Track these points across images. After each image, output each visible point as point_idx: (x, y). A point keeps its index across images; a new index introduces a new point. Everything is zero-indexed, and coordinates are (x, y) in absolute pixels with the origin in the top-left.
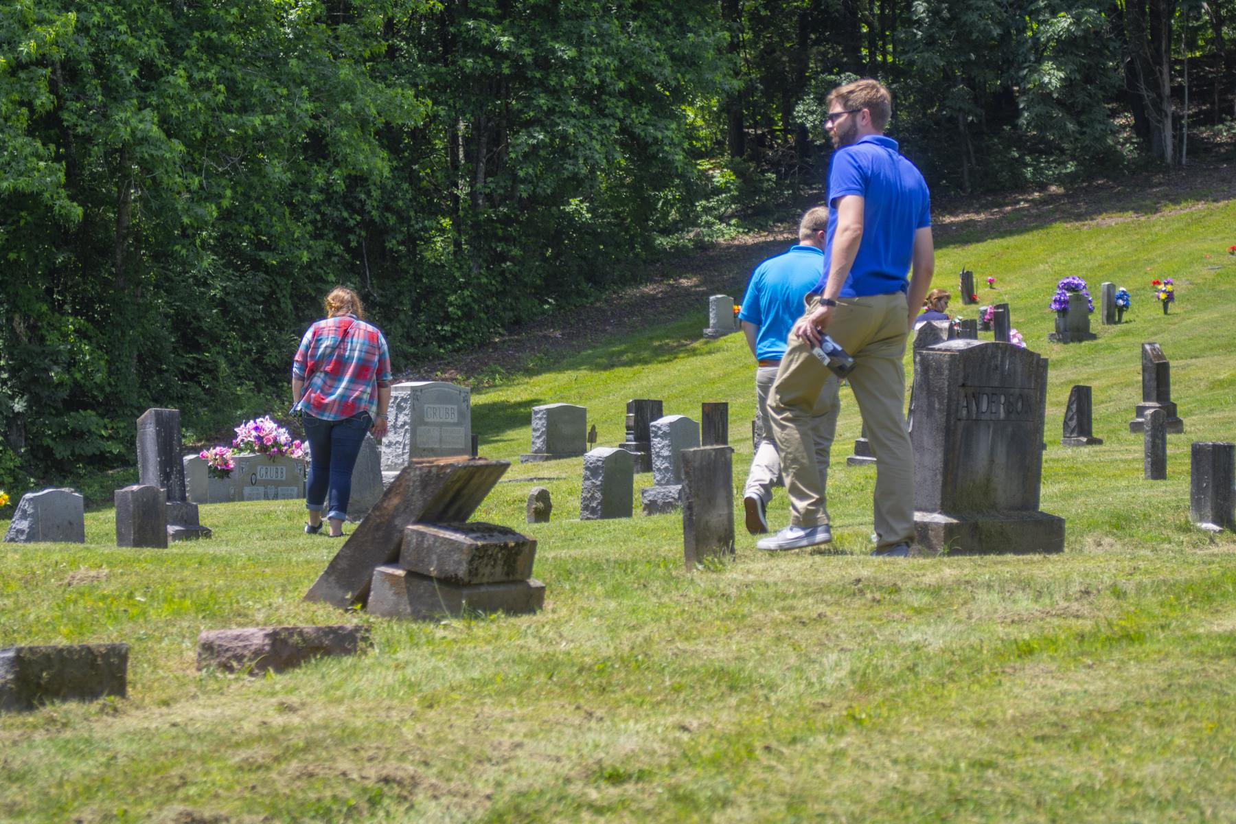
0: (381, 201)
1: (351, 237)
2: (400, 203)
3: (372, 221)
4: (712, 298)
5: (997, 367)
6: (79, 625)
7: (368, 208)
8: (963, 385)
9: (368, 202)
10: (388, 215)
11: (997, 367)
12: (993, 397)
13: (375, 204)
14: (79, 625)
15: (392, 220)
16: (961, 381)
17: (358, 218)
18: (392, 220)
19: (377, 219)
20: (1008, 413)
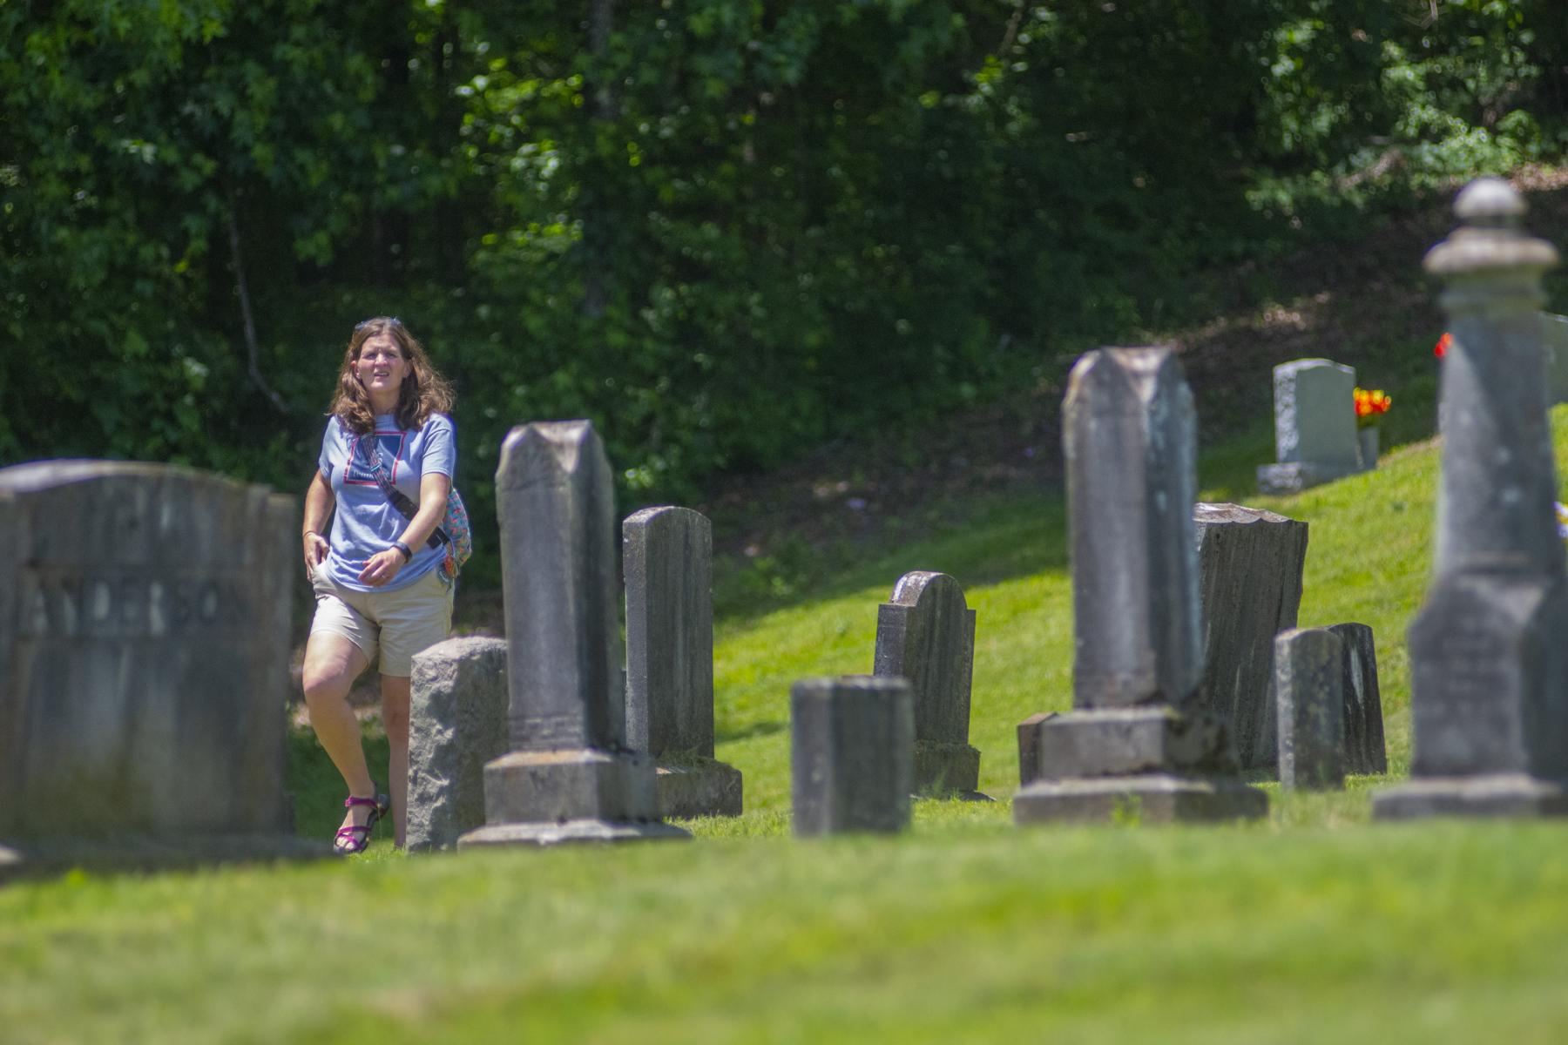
0: (274, 113)
1: (193, 223)
2: (337, 121)
3: (254, 177)
4: (1286, 370)
5: (133, 524)
6: (1385, 663)
7: (240, 134)
8: (34, 563)
9: (241, 116)
10: (303, 156)
11: (133, 524)
12: (127, 587)
13: (261, 121)
14: (1385, 663)
15: (316, 170)
16: (24, 552)
17: (209, 166)
18: (316, 170)
19: (271, 172)
20: (177, 623)
